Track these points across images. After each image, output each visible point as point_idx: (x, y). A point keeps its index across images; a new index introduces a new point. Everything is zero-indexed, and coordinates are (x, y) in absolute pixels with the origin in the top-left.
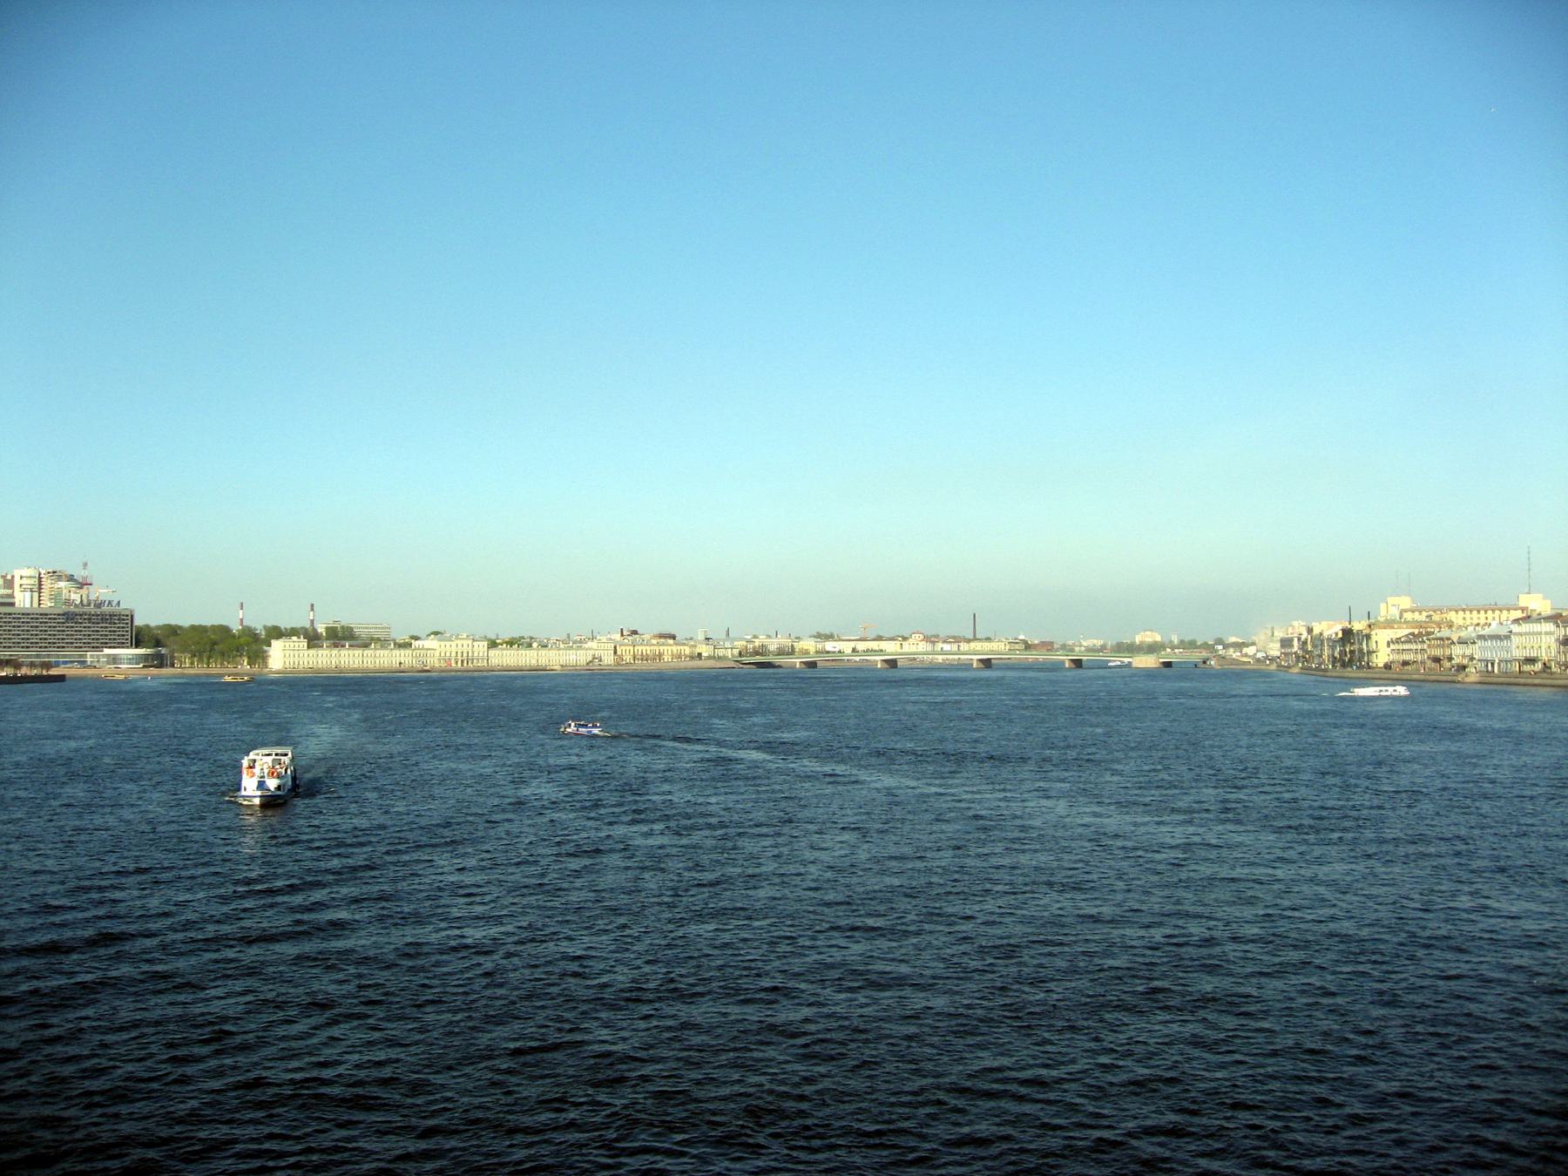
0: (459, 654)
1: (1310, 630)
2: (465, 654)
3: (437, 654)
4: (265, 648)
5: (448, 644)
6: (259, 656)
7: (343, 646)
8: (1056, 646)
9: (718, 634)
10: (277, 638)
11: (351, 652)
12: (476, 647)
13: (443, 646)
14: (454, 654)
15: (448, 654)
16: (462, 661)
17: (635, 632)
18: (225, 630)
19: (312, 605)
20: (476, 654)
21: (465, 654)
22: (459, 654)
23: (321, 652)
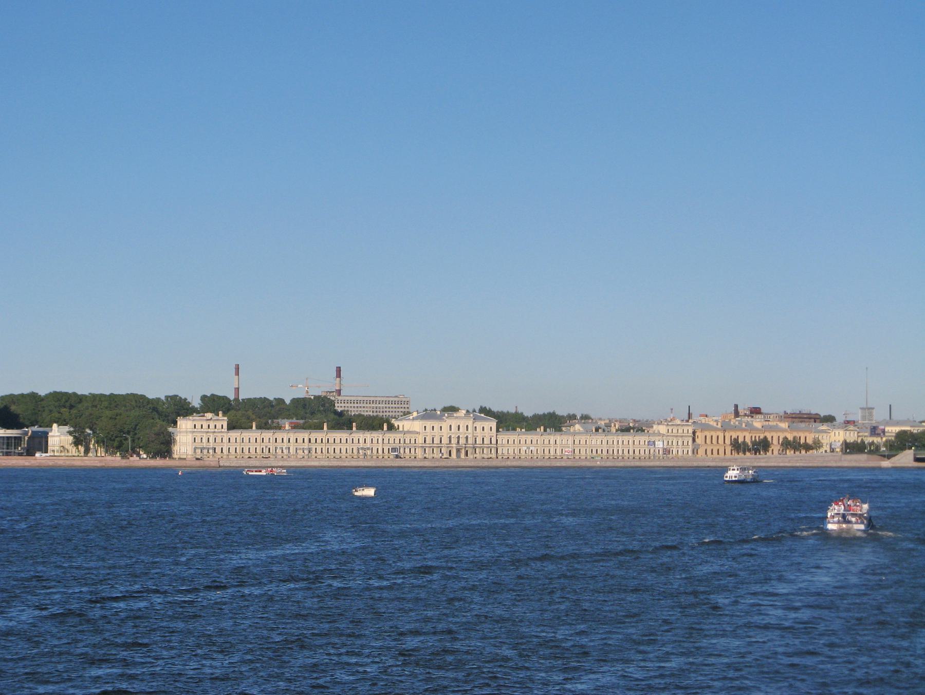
0: (454, 441)
1: (87, 451)
2: (462, 441)
3: (420, 440)
4: (170, 429)
5: (437, 424)
6: (164, 447)
7: (279, 428)
8: (841, 609)
9: (879, 415)
10: (184, 416)
11: (293, 436)
12: (479, 429)
13: (429, 429)
14: (445, 441)
15: (437, 441)
16: (458, 451)
17: (756, 411)
18: (281, 401)
19: (339, 370)
20: (479, 441)
21: (462, 441)
22: (454, 441)
23: (279, 435)
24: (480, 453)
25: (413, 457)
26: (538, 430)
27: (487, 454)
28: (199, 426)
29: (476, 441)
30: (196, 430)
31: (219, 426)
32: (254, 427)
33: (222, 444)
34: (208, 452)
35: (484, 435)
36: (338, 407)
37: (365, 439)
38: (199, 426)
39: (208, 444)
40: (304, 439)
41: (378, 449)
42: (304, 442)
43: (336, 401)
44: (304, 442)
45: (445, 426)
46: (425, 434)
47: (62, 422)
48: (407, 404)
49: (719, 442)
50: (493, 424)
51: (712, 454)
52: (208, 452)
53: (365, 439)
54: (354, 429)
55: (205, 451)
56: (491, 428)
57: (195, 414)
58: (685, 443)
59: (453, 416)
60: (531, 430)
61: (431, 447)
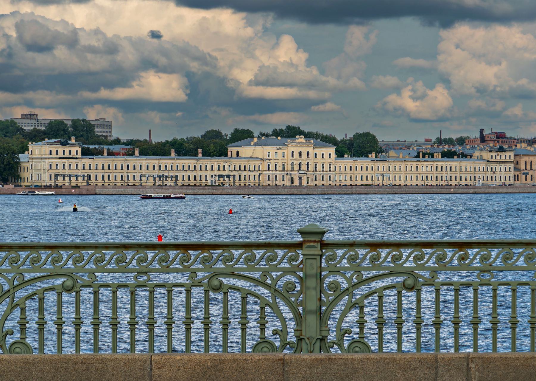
24: (319, 179)
25: (257, 185)
26: (370, 156)
27: (280, 182)
28: (54, 152)
29: (316, 168)
30: (51, 156)
31: (74, 152)
32: (137, 152)
33: (432, 172)
34: (64, 180)
35: (324, 161)
36: (98, 132)
37: (212, 166)
38: (54, 152)
39: (64, 171)
40: (154, 166)
41: (134, 176)
42: (154, 169)
43: (96, 126)
44: (154, 169)
45: (280, 153)
46: (330, 161)
47: (200, 148)
48: (110, 128)
49: (527, 168)
50: (332, 150)
51: (362, 180)
52: (64, 180)
53: (212, 166)
54: (200, 155)
55: (60, 178)
56: (330, 155)
57: (297, 137)
58: (508, 170)
59: (295, 142)
60: (220, 156)
61: (282, 174)
